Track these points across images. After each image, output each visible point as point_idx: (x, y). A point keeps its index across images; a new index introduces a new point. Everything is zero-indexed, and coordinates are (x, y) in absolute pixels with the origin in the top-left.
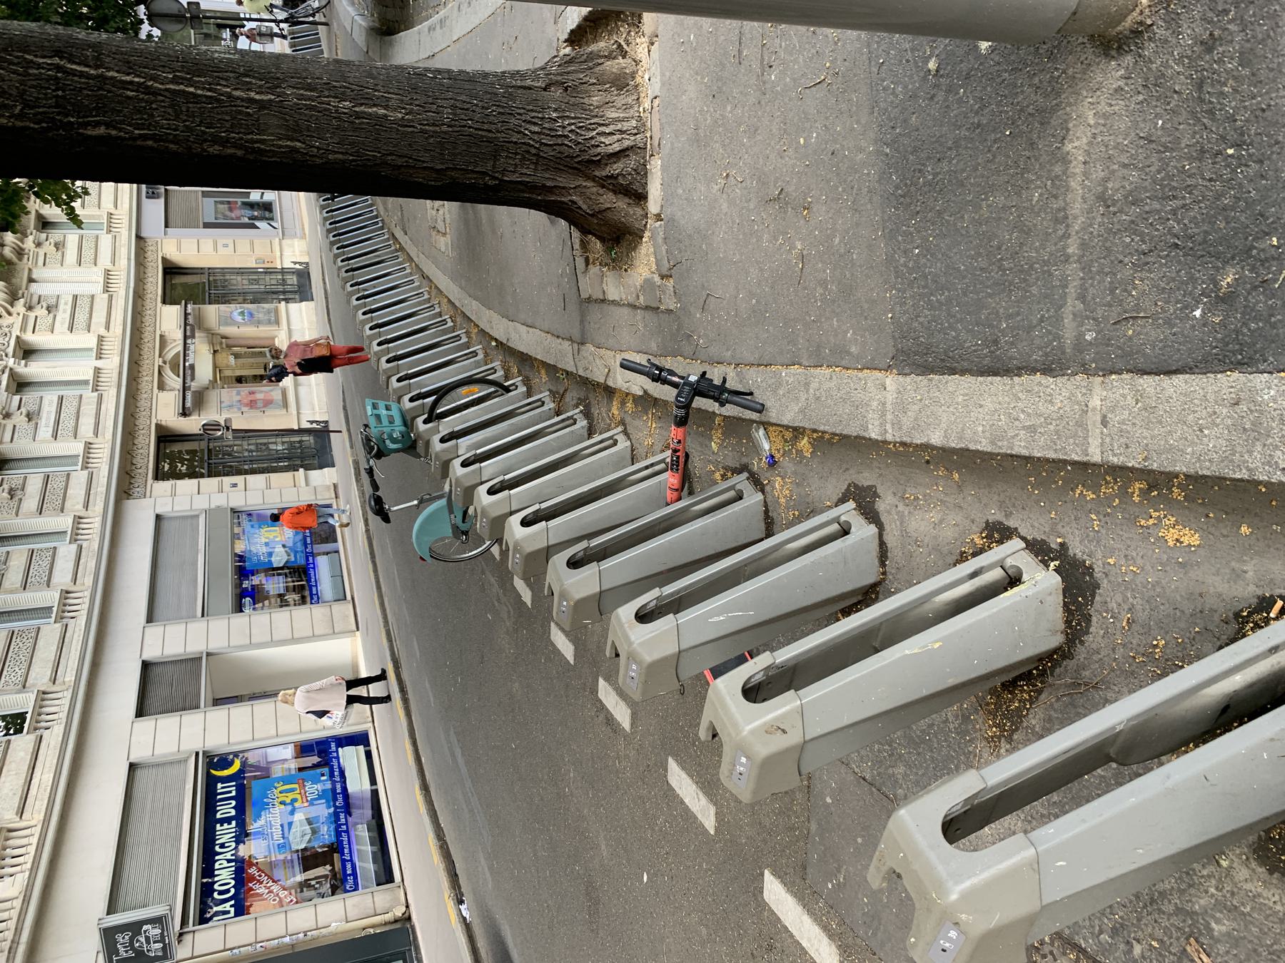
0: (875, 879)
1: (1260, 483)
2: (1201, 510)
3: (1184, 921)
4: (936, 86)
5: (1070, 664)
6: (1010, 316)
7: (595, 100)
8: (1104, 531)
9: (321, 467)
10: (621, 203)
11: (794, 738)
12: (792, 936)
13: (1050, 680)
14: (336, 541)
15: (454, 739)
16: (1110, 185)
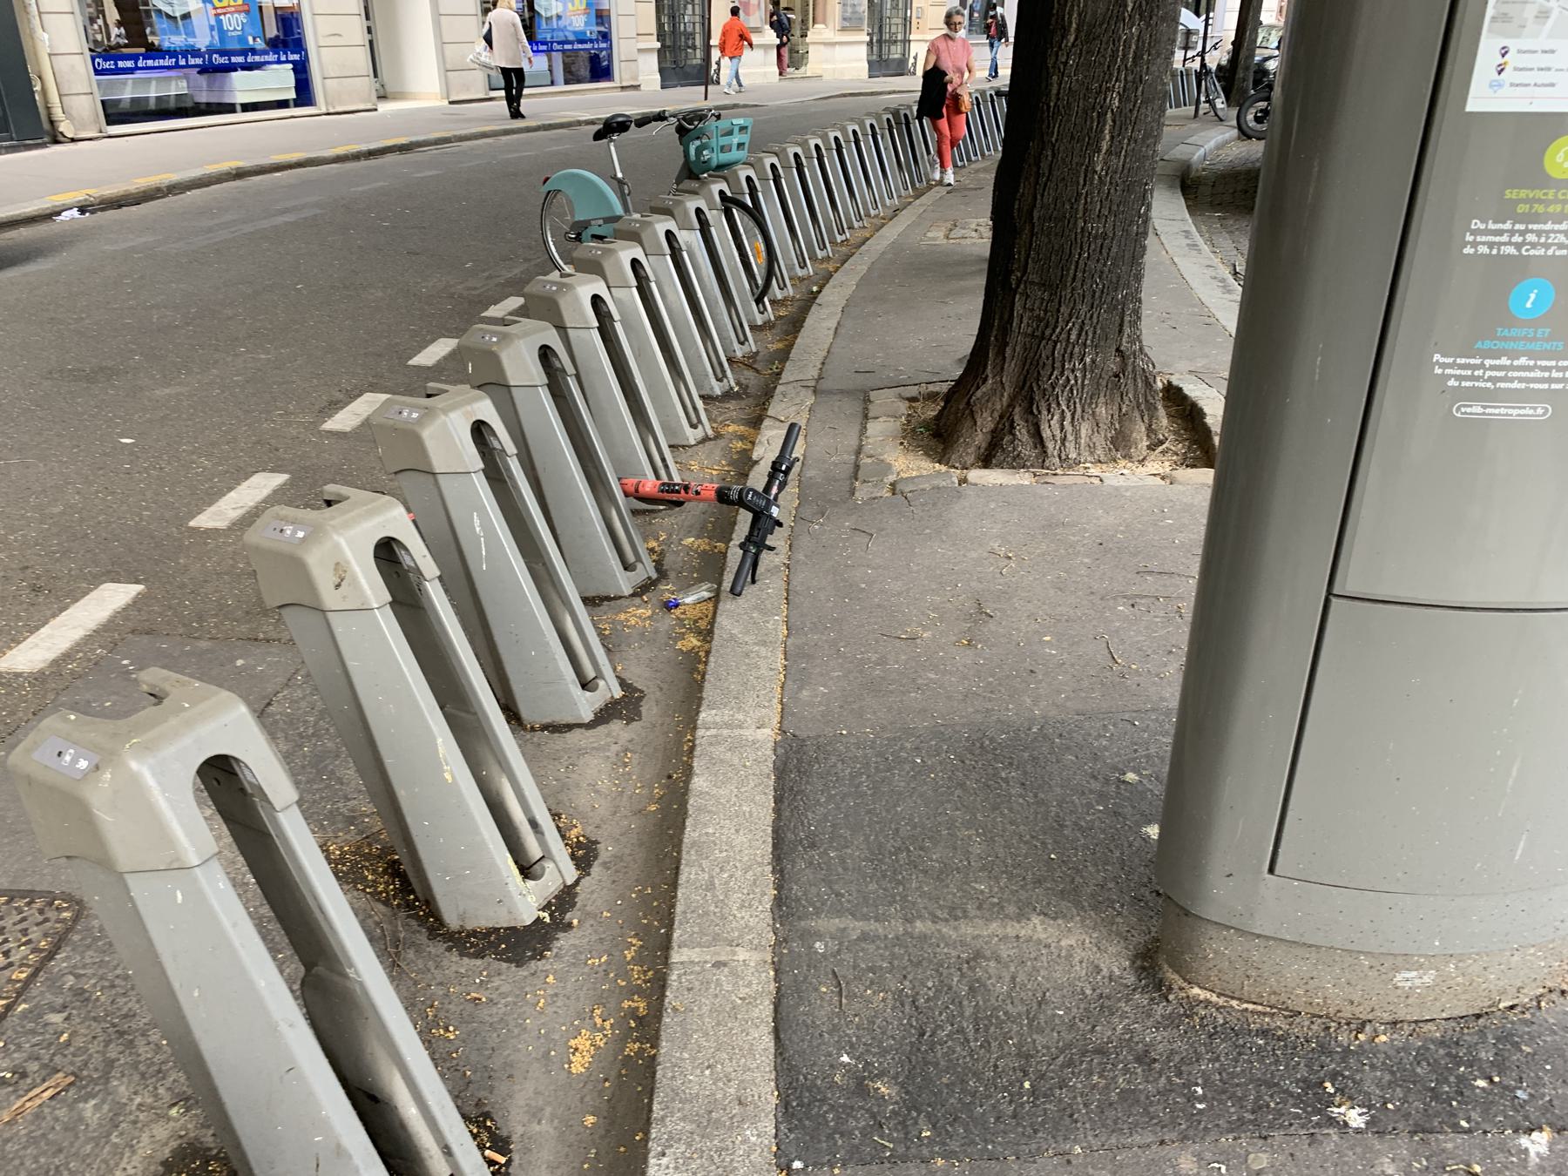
0: (153, 676)
1: (647, 1133)
2: (613, 1073)
3: (96, 1070)
4: (1107, 781)
5: (422, 937)
6: (843, 861)
7: (1102, 411)
8: (586, 970)
9: (661, 71)
10: (980, 438)
11: (330, 598)
12: (54, 616)
13: (402, 914)
14: (567, 82)
15: (307, 213)
16: (992, 964)
